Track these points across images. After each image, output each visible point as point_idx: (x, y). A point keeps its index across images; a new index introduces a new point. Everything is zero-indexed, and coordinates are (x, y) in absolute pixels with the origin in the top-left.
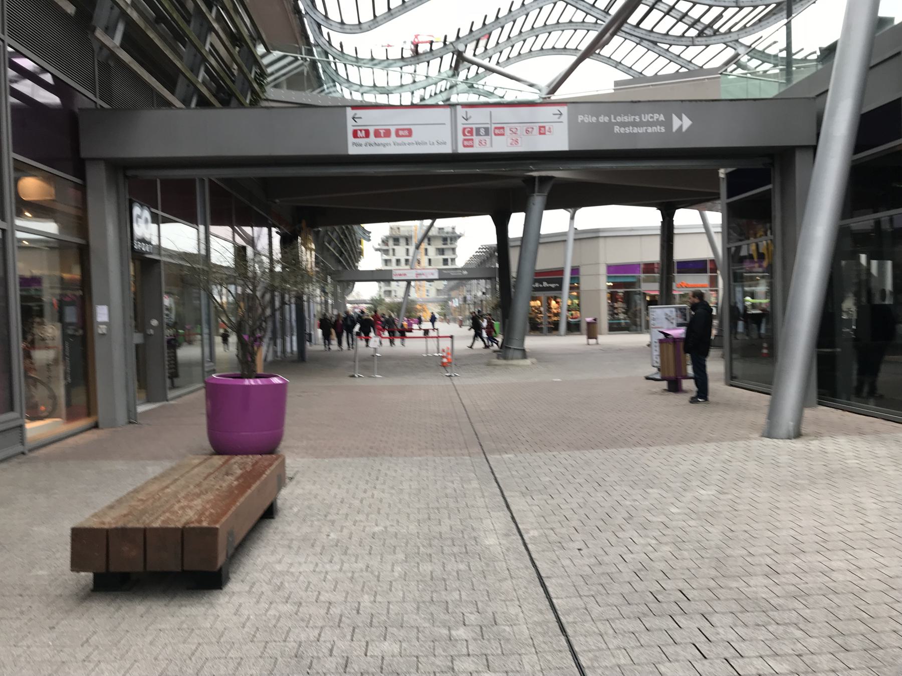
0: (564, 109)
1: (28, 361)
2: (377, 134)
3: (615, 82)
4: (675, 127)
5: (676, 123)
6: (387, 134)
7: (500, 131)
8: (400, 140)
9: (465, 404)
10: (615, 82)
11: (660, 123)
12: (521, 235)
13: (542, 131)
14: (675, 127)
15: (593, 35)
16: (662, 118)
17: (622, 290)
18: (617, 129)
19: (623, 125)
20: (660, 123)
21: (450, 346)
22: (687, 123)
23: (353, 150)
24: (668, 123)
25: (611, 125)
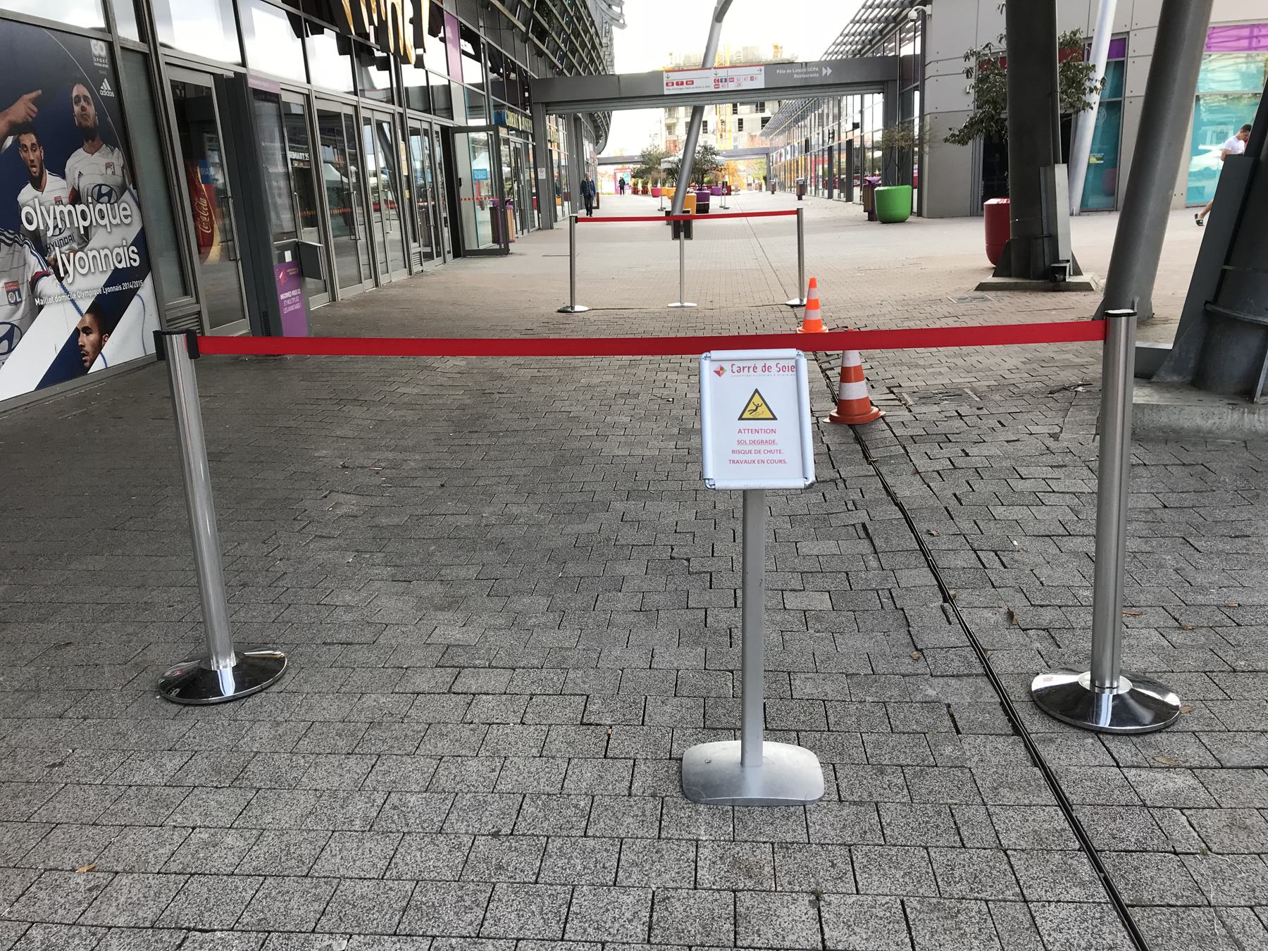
0: (763, 68)
1: (87, 341)
2: (677, 84)
3: (340, 54)
4: (823, 74)
5: (824, 71)
6: (682, 84)
7: (732, 80)
8: (678, 87)
9: (926, 571)
10: (340, 54)
11: (816, 72)
12: (293, 112)
13: (752, 79)
14: (823, 74)
15: (918, 40)
16: (817, 69)
17: (347, 150)
18: (795, 76)
19: (797, 73)
20: (816, 72)
21: (1096, 370)
22: (829, 71)
23: (666, 93)
24: (821, 71)
25: (792, 74)
